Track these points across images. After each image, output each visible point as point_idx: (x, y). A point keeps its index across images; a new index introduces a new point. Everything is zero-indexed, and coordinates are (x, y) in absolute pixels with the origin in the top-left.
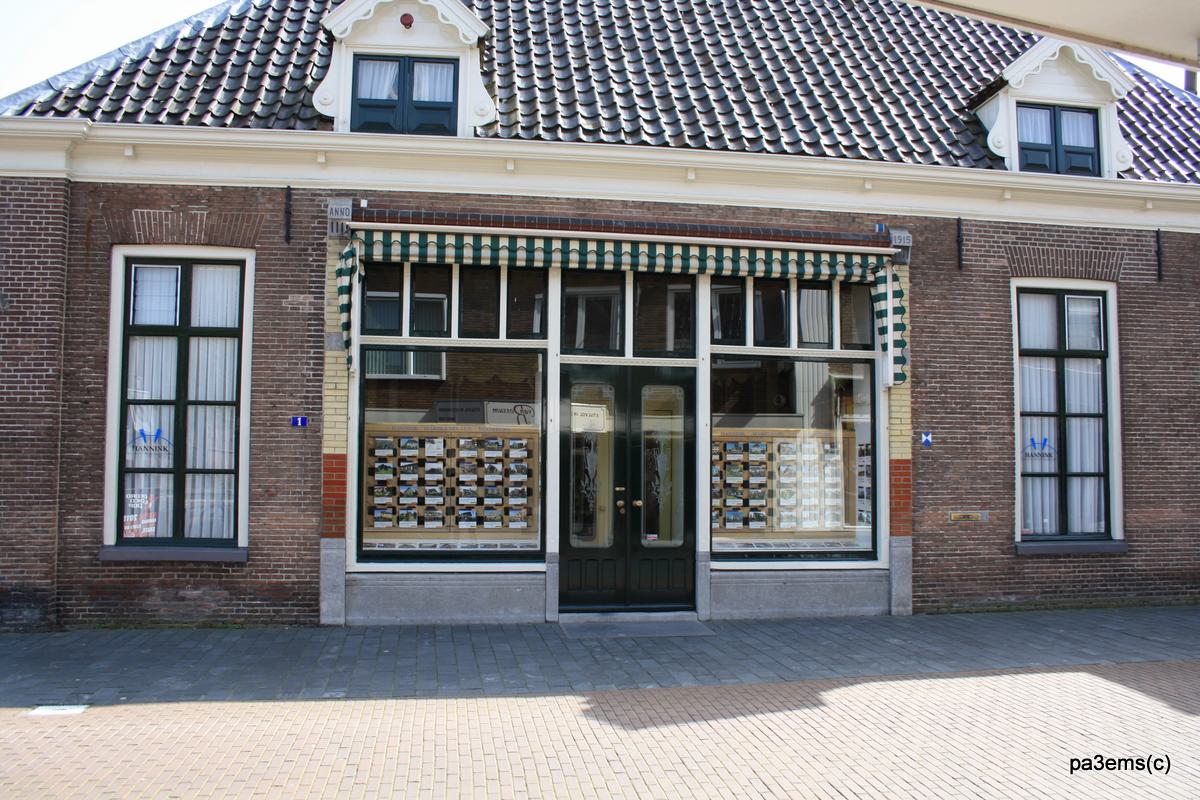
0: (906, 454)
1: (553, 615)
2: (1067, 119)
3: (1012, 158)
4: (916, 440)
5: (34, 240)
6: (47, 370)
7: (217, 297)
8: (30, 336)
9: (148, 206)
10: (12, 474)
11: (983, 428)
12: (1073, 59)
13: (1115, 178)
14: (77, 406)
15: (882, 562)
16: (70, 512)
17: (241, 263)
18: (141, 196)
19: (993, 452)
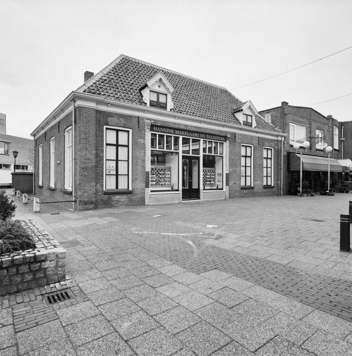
0: (228, 172)
1: (181, 201)
2: (161, 96)
3: (242, 124)
4: (229, 170)
5: (90, 122)
6: (93, 152)
7: (123, 138)
8: (89, 144)
9: (112, 117)
10: (87, 175)
11: (237, 168)
12: (162, 81)
13: (169, 110)
14: (98, 160)
15: (224, 190)
16: (97, 184)
17: (128, 132)
18: (110, 115)
19: (239, 172)
